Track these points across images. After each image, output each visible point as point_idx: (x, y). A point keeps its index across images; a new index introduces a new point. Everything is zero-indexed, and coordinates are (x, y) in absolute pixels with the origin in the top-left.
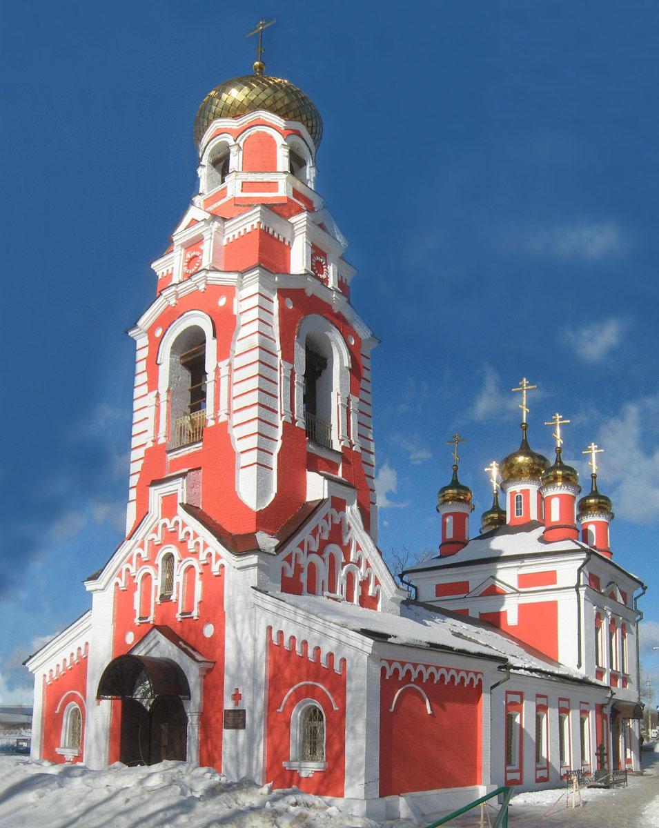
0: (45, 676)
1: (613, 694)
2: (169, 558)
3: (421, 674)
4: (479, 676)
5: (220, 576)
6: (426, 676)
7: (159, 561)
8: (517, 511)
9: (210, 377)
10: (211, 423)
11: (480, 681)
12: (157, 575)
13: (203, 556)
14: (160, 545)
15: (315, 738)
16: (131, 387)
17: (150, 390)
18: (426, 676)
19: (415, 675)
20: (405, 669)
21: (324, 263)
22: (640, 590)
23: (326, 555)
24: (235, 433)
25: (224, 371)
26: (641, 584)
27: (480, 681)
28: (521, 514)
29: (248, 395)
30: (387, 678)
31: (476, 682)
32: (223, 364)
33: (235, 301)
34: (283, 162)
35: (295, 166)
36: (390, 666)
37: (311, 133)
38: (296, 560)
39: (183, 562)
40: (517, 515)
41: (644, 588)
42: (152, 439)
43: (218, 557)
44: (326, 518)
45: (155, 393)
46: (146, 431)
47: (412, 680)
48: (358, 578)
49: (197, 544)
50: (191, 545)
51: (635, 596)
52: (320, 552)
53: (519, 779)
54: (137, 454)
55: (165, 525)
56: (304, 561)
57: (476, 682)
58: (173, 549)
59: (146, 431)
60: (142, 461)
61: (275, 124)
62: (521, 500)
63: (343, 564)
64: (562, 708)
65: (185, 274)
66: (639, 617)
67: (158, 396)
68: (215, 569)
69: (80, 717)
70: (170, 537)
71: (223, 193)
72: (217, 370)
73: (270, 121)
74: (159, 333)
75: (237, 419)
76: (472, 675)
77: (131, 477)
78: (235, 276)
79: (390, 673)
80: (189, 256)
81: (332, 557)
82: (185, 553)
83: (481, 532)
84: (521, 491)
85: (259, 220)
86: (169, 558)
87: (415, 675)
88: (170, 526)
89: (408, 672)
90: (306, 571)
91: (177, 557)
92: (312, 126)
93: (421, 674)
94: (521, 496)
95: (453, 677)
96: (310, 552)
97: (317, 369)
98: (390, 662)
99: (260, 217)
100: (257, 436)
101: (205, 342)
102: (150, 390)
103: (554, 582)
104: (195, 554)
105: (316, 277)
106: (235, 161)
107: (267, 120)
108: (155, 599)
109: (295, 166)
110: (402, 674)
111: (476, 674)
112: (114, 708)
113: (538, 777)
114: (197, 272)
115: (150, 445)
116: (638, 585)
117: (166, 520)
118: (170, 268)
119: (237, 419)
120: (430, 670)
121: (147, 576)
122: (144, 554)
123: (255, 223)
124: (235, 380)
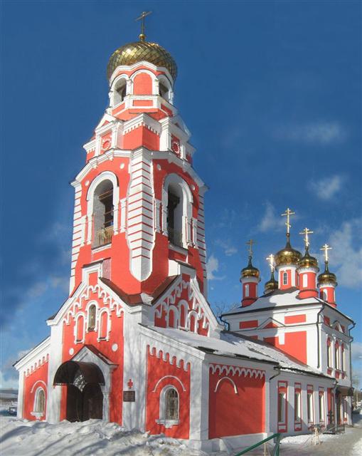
1: (337, 382)
7: (87, 309)
9: (116, 207)
10: (116, 233)
13: (112, 307)
16: (72, 213)
17: (82, 215)
19: (228, 372)
22: (352, 325)
23: (179, 306)
24: (129, 239)
25: (123, 204)
32: (123, 201)
33: (129, 166)
37: (171, 74)
43: (120, 307)
44: (179, 285)
48: (197, 319)
52: (176, 304)
56: (167, 309)
57: (262, 376)
58: (95, 303)
63: (189, 311)
67: (87, 218)
68: (118, 313)
69: (44, 395)
72: (120, 204)
74: (87, 184)
76: (238, 369)
78: (129, 152)
79: (214, 371)
80: (104, 141)
81: (182, 307)
87: (228, 372)
89: (225, 371)
91: (97, 307)
96: (170, 304)
97: (174, 203)
98: (215, 365)
102: (82, 215)
104: (107, 305)
110: (221, 371)
112: (63, 390)
115: (83, 245)
117: (92, 287)
120: (249, 370)
124: (129, 209)
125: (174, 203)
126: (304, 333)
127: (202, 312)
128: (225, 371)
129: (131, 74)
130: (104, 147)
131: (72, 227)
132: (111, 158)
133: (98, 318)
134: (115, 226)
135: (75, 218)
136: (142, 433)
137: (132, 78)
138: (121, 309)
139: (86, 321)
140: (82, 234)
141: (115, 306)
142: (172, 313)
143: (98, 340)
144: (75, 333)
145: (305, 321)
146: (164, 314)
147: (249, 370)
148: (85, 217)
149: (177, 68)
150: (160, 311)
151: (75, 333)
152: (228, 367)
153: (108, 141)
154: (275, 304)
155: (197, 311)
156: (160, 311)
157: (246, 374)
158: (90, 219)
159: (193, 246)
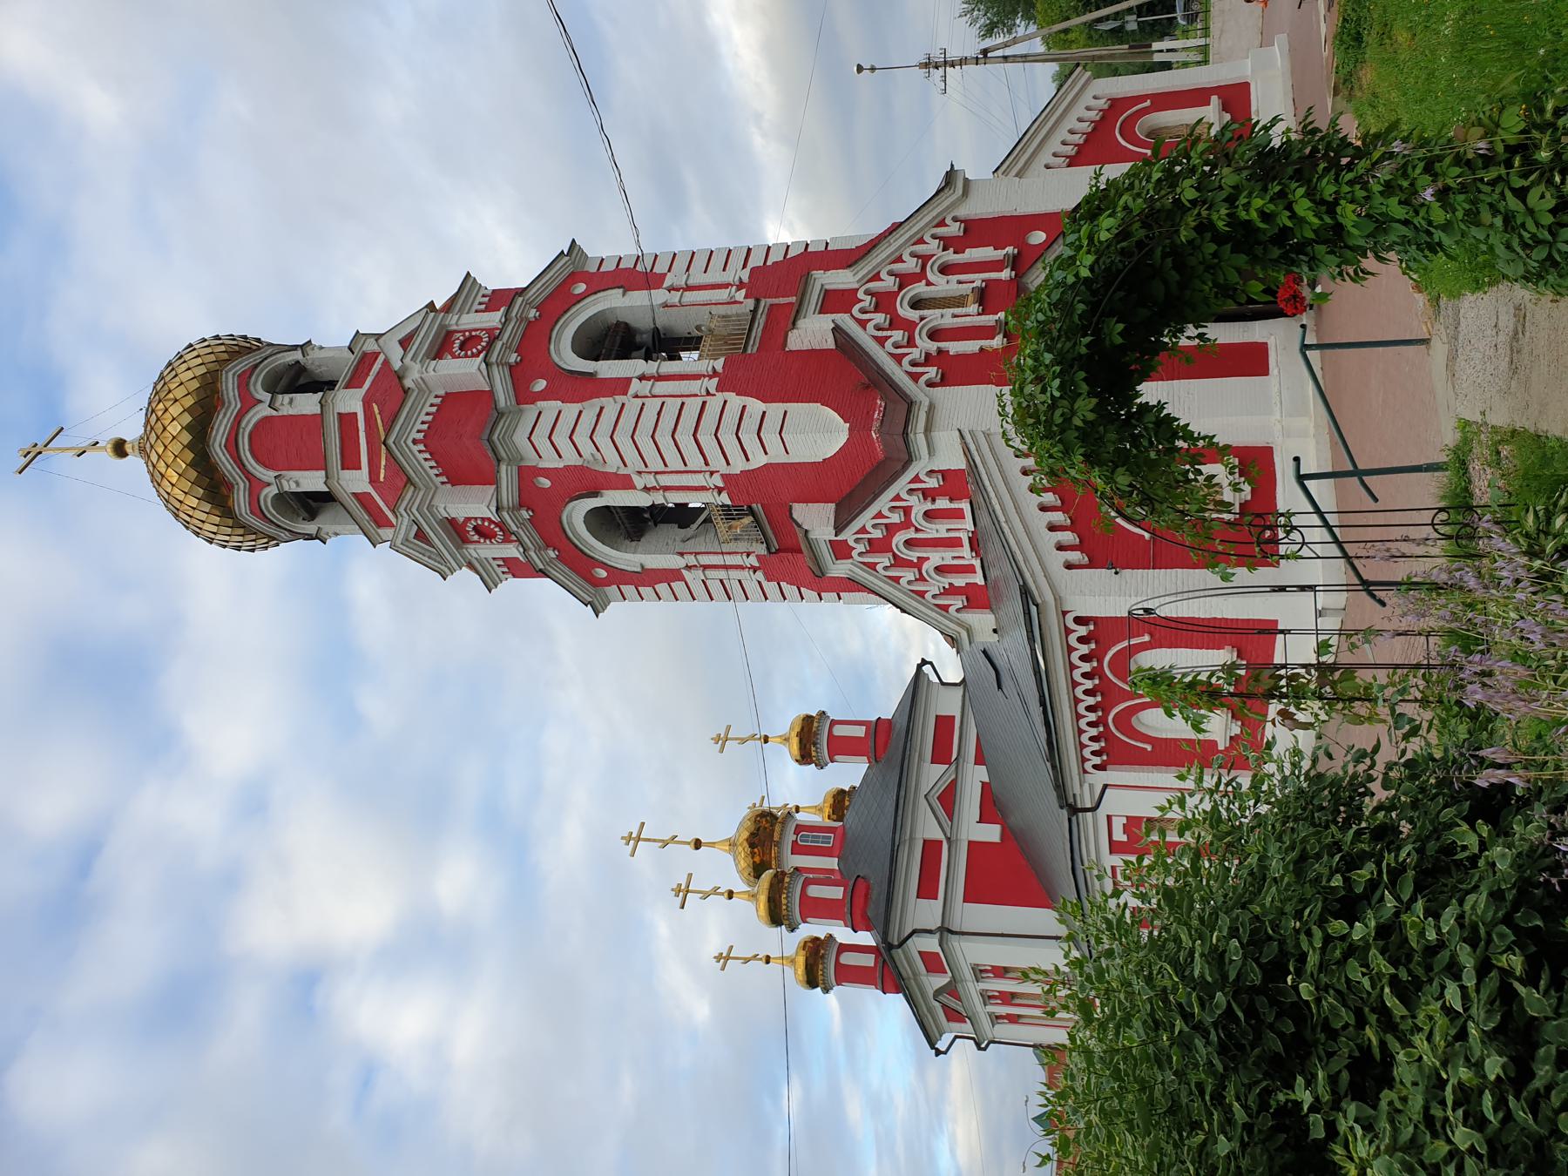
0: (1069, 566)
2: (916, 304)
5: (945, 474)
7: (913, 555)
9: (658, 498)
10: (725, 499)
13: (913, 501)
14: (895, 555)
20: (1082, 697)
24: (738, 465)
25: (650, 481)
32: (639, 482)
33: (542, 465)
34: (306, 404)
35: (302, 381)
41: (924, 662)
43: (916, 479)
49: (874, 526)
50: (896, 518)
52: (909, 326)
58: (899, 539)
63: (929, 284)
65: (506, 540)
67: (688, 567)
68: (932, 483)
70: (876, 546)
71: (361, 498)
72: (646, 489)
74: (603, 573)
75: (717, 462)
78: (503, 468)
80: (476, 538)
84: (796, 833)
86: (916, 304)
88: (861, 548)
91: (910, 534)
96: (922, 579)
101: (607, 507)
102: (682, 579)
104: (907, 511)
105: (489, 348)
106: (312, 481)
115: (760, 575)
117: (854, 553)
118: (494, 563)
119: (717, 462)
121: (940, 570)
122: (908, 575)
124: (661, 467)
129: (255, 485)
130: (494, 535)
132: (525, 514)
136: (1537, 989)
137: (267, 475)
141: (911, 491)
144: (971, 346)
148: (684, 572)
151: (971, 346)
153: (475, 528)
154: (1276, 622)
158: (691, 560)
159: (715, 373)
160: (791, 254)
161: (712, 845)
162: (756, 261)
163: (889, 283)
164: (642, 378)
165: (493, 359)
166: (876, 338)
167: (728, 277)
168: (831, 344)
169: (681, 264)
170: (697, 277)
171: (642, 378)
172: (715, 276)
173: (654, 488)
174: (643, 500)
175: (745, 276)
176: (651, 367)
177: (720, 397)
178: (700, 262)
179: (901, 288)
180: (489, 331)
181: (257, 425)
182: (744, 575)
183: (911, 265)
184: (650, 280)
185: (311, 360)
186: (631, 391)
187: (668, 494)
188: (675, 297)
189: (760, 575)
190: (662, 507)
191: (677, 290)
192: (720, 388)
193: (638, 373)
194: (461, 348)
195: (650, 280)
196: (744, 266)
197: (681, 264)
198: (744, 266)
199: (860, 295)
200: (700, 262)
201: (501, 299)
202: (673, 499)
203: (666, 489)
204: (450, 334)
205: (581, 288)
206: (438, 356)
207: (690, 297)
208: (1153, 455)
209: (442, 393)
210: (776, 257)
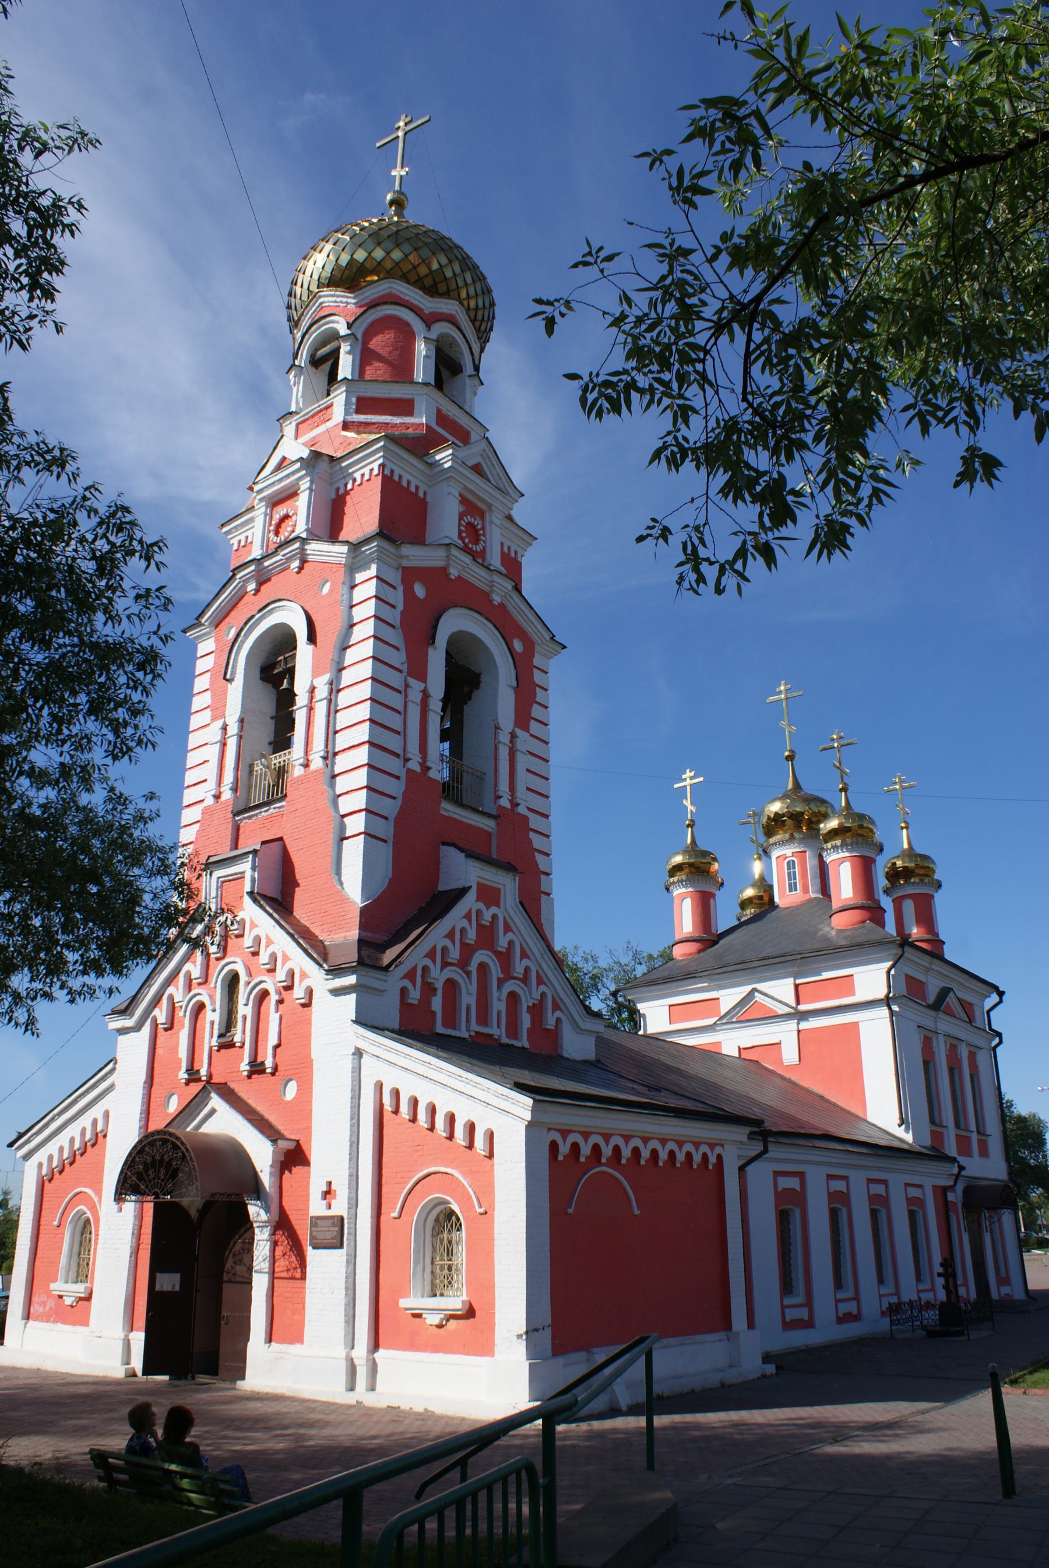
1: (961, 1168)
3: (617, 1149)
4: (718, 1150)
6: (626, 1153)
8: (790, 885)
9: (301, 700)
11: (719, 1157)
12: (213, 1002)
15: (450, 1260)
16: (187, 713)
17: (214, 719)
18: (626, 1153)
19: (607, 1151)
21: (479, 527)
22: (994, 998)
23: (473, 967)
26: (996, 988)
27: (719, 1157)
28: (796, 890)
29: (39, 1248)
30: (561, 1158)
31: (713, 1159)
34: (422, 369)
35: (445, 372)
36: (627, 1143)
37: (473, 321)
38: (423, 976)
39: (251, 985)
40: (790, 891)
41: (1001, 994)
42: (213, 792)
44: (468, 916)
45: (219, 723)
46: (205, 781)
47: (604, 1160)
48: (526, 1002)
51: (986, 1008)
52: (463, 963)
53: (806, 1318)
54: (188, 816)
55: (479, 913)
56: (439, 977)
57: (713, 1159)
59: (205, 781)
60: (197, 826)
61: (415, 302)
62: (794, 868)
63: (501, 982)
64: (835, 1192)
66: (997, 1040)
67: (224, 728)
69: (85, 1230)
72: (312, 690)
73: (407, 298)
76: (704, 1148)
77: (182, 831)
79: (564, 1149)
80: (277, 517)
81: (483, 967)
82: (507, 974)
83: (739, 919)
85: (381, 461)
87: (607, 1151)
89: (596, 1148)
90: (440, 992)
92: (477, 308)
93: (617, 1149)
94: (793, 862)
95: (689, 1155)
96: (445, 964)
97: (466, 689)
98: (565, 1133)
99: (383, 456)
100: (365, 790)
102: (214, 719)
103: (852, 992)
105: (466, 550)
106: (346, 368)
107: (402, 296)
108: (210, 1042)
109: (445, 372)
110: (586, 1150)
111: (712, 1146)
112: (140, 1217)
113: (840, 1315)
114: (288, 542)
116: (992, 990)
120: (572, 1138)
122: (455, 954)
123: (375, 466)
125: (466, 689)
126: (856, 1025)
127: (540, 981)
128: (596, 1148)
131: (184, 751)
133: (244, 1010)
134: (297, 750)
135: (193, 726)
138: (307, 983)
139: (213, 1016)
140: (210, 772)
142: (451, 985)
143: (102, 1485)
145: (853, 994)
146: (429, 989)
147: (595, 1139)
149: (492, 304)
150: (434, 962)
152: (607, 1137)
155: (525, 979)
156: (434, 962)
157: (697, 1158)
158: (233, 729)
160: (539, 857)
161: (749, 286)
162: (535, 822)
163: (503, 942)
164: (426, 695)
165: (454, 551)
166: (414, 969)
167: (521, 793)
168: (441, 887)
169: (537, 747)
170: (523, 762)
171: (426, 695)
172: (523, 779)
173: (312, 698)
174: (301, 687)
175: (522, 810)
176: (436, 705)
177: (403, 774)
178: (537, 765)
179: (497, 954)
180: (483, 553)
181: (408, 324)
182: (211, 785)
183: (519, 968)
184: (523, 719)
185: (465, 379)
186: (412, 681)
187: (304, 710)
188: (504, 738)
189: (210, 801)
190: (292, 702)
191: (511, 742)
192: (410, 772)
193: (431, 691)
194: (469, 524)
195: (523, 719)
196: (529, 809)
197: (537, 747)
198: (529, 809)
199: (494, 910)
200: (537, 765)
201: (512, 568)
202: (300, 718)
203: (311, 709)
204: (481, 514)
205: (518, 646)
206: (463, 500)
207: (504, 753)
208: (792, 351)
209: (428, 499)
210: (537, 841)
